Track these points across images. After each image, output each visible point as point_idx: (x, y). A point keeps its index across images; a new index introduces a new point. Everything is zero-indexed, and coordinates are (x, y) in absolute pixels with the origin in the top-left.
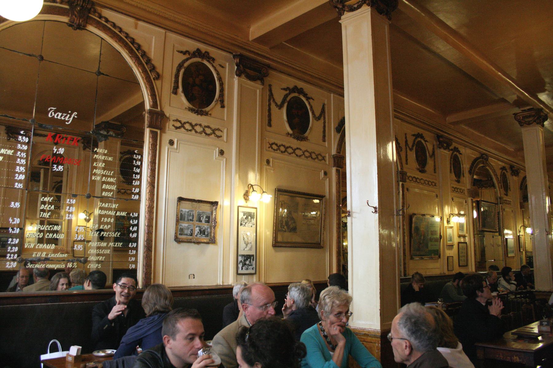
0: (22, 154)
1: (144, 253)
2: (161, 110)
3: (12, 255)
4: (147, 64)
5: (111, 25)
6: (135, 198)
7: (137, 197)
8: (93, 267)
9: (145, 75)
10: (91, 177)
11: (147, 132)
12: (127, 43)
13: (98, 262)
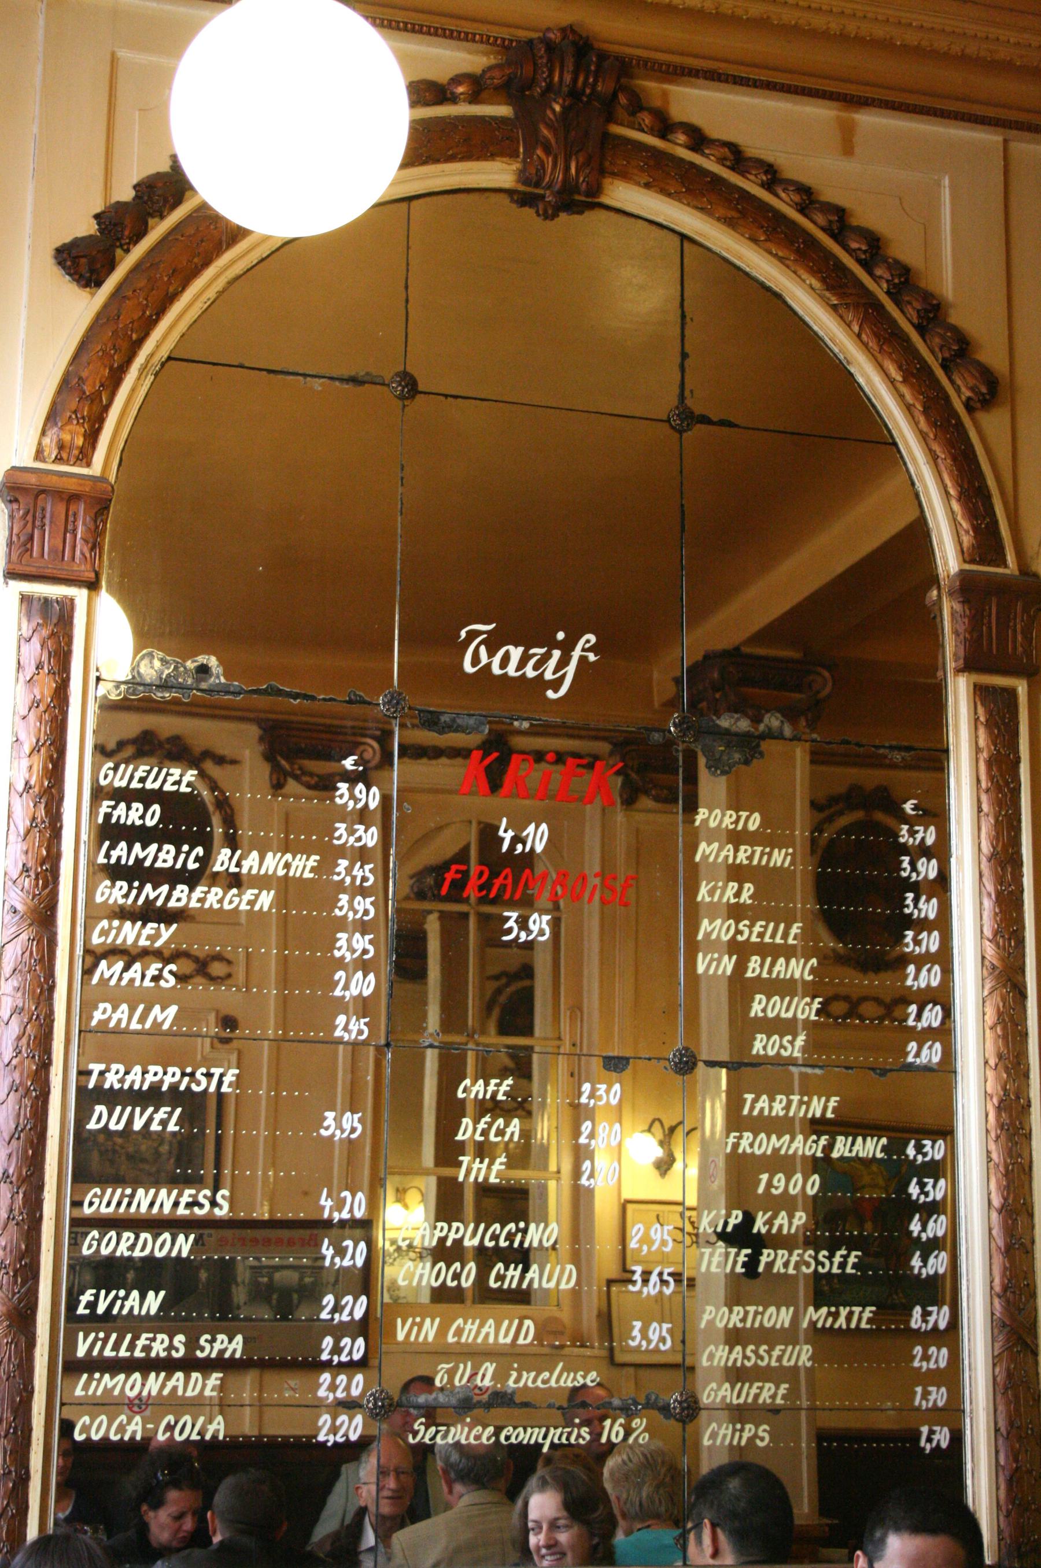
0: (357, 872)
1: (996, 1360)
2: (1024, 570)
3: (342, 1379)
4: (867, 266)
5: (721, 161)
6: (923, 1059)
7: (932, 1054)
8: (717, 1438)
9: (917, 391)
10: (691, 963)
11: (960, 695)
12: (812, 242)
13: (740, 1414)
